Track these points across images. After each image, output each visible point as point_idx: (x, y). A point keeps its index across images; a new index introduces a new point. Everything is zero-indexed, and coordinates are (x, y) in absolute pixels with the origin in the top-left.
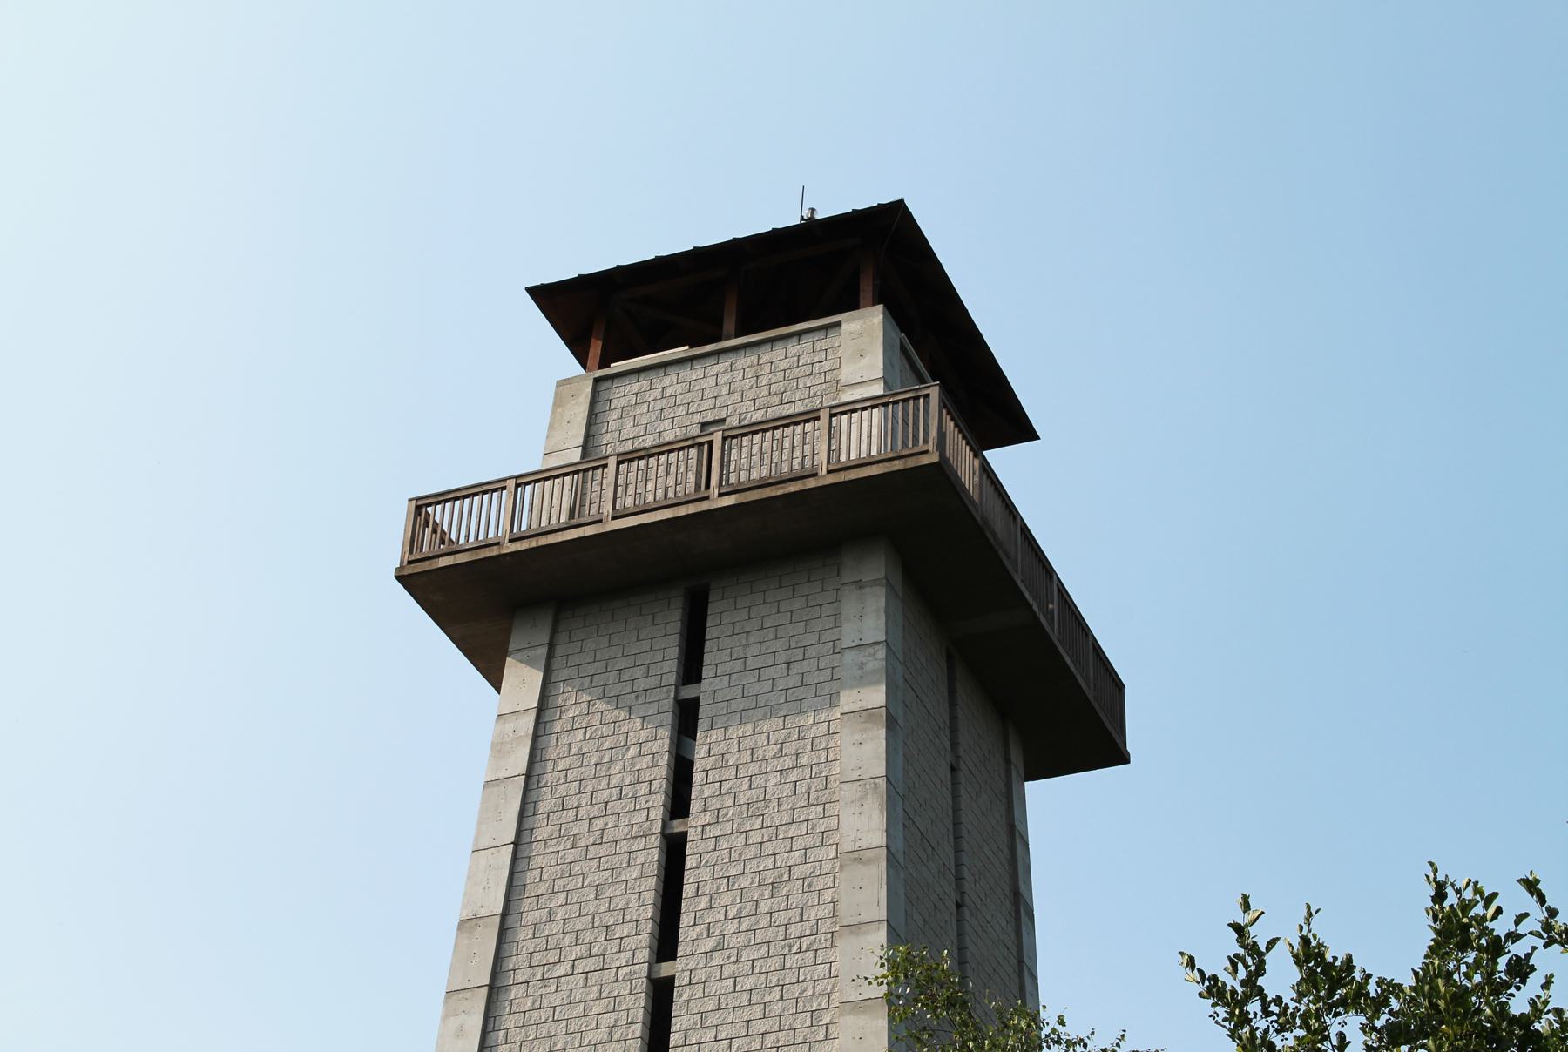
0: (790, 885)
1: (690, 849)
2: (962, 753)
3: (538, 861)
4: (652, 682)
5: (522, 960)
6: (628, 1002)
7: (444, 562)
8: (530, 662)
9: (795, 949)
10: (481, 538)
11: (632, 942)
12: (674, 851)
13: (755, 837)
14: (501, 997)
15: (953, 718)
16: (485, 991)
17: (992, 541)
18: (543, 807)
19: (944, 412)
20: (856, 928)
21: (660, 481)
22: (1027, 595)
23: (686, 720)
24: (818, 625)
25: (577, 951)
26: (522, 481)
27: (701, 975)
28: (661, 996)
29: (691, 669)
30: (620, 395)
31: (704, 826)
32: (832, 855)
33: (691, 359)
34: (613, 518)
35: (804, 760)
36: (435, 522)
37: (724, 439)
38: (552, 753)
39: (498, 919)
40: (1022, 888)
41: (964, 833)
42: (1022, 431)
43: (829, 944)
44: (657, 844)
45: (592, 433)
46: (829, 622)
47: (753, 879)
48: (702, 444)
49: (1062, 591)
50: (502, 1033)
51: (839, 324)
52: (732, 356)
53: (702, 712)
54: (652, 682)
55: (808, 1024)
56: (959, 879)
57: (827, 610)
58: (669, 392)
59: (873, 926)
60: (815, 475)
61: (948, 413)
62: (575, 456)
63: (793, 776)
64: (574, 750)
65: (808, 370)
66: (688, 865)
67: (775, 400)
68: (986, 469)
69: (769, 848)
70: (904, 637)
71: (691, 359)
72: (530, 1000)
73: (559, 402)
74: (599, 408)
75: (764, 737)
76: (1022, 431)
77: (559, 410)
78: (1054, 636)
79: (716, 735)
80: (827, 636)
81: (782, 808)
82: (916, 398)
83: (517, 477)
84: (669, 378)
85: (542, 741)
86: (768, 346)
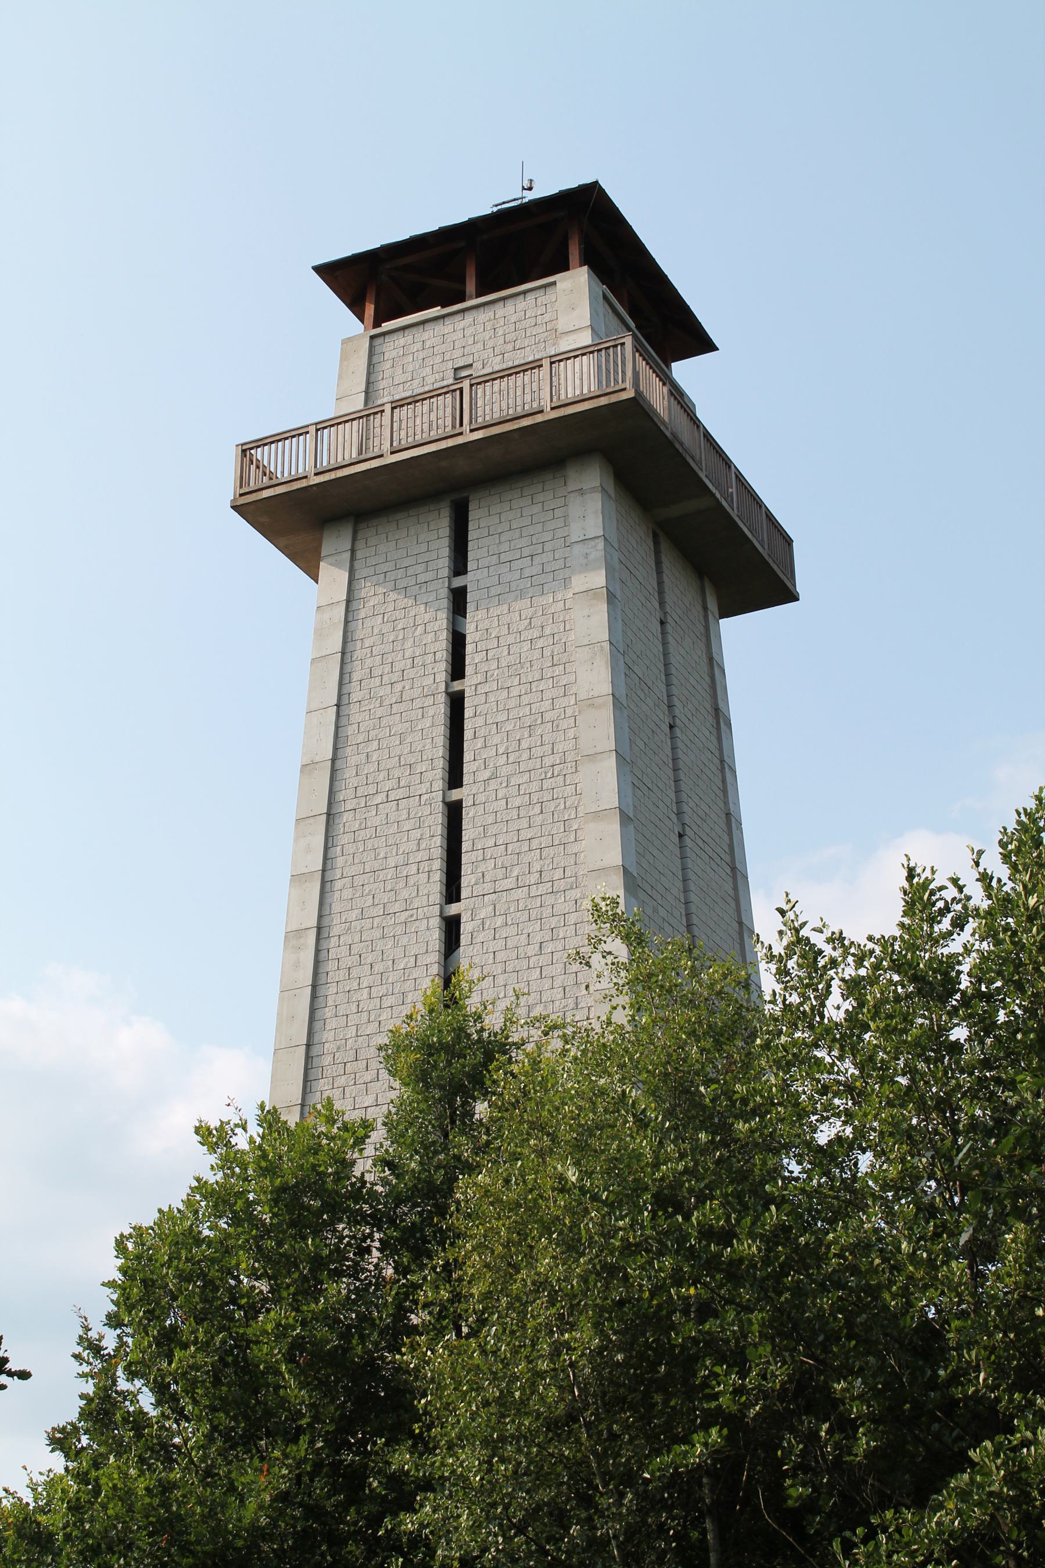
0: (543, 726)
1: (467, 703)
2: (668, 609)
3: (355, 718)
4: (430, 576)
5: (350, 793)
6: (430, 821)
7: (266, 494)
8: (338, 565)
9: (549, 775)
10: (293, 473)
11: (429, 776)
12: (456, 704)
13: (515, 692)
14: (336, 822)
15: (660, 583)
16: (324, 817)
17: (681, 450)
18: (356, 676)
19: (637, 354)
20: (592, 757)
21: (426, 417)
22: (711, 486)
23: (458, 601)
24: (551, 525)
25: (389, 785)
26: (321, 427)
27: (481, 798)
28: (454, 813)
29: (460, 564)
30: (392, 347)
31: (476, 685)
32: (573, 702)
33: (443, 317)
34: (392, 453)
35: (548, 631)
36: (257, 460)
37: (471, 385)
38: (359, 634)
39: (330, 763)
40: (721, 705)
41: (673, 671)
42: (702, 344)
43: (574, 770)
44: (443, 700)
45: (371, 380)
46: (560, 523)
47: (515, 724)
48: (454, 391)
49: (740, 479)
50: (339, 848)
51: (554, 283)
52: (474, 312)
53: (469, 597)
54: (430, 576)
55: (562, 830)
56: (670, 706)
57: (558, 513)
58: (428, 344)
59: (606, 755)
60: (542, 412)
61: (641, 355)
62: (360, 405)
63: (540, 643)
64: (376, 631)
65: (533, 321)
66: (466, 716)
67: (510, 347)
68: (677, 393)
69: (525, 700)
70: (618, 529)
71: (443, 317)
72: (358, 822)
73: (344, 357)
74: (375, 359)
75: (517, 614)
76: (702, 344)
77: (345, 363)
78: (734, 514)
79: (481, 614)
80: (560, 533)
81: (534, 668)
82: (615, 346)
83: (316, 424)
84: (427, 333)
85: (352, 626)
86: (501, 304)
